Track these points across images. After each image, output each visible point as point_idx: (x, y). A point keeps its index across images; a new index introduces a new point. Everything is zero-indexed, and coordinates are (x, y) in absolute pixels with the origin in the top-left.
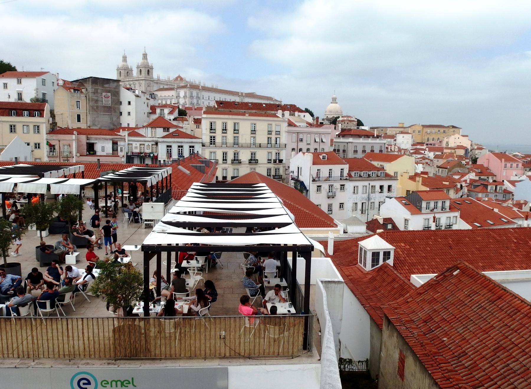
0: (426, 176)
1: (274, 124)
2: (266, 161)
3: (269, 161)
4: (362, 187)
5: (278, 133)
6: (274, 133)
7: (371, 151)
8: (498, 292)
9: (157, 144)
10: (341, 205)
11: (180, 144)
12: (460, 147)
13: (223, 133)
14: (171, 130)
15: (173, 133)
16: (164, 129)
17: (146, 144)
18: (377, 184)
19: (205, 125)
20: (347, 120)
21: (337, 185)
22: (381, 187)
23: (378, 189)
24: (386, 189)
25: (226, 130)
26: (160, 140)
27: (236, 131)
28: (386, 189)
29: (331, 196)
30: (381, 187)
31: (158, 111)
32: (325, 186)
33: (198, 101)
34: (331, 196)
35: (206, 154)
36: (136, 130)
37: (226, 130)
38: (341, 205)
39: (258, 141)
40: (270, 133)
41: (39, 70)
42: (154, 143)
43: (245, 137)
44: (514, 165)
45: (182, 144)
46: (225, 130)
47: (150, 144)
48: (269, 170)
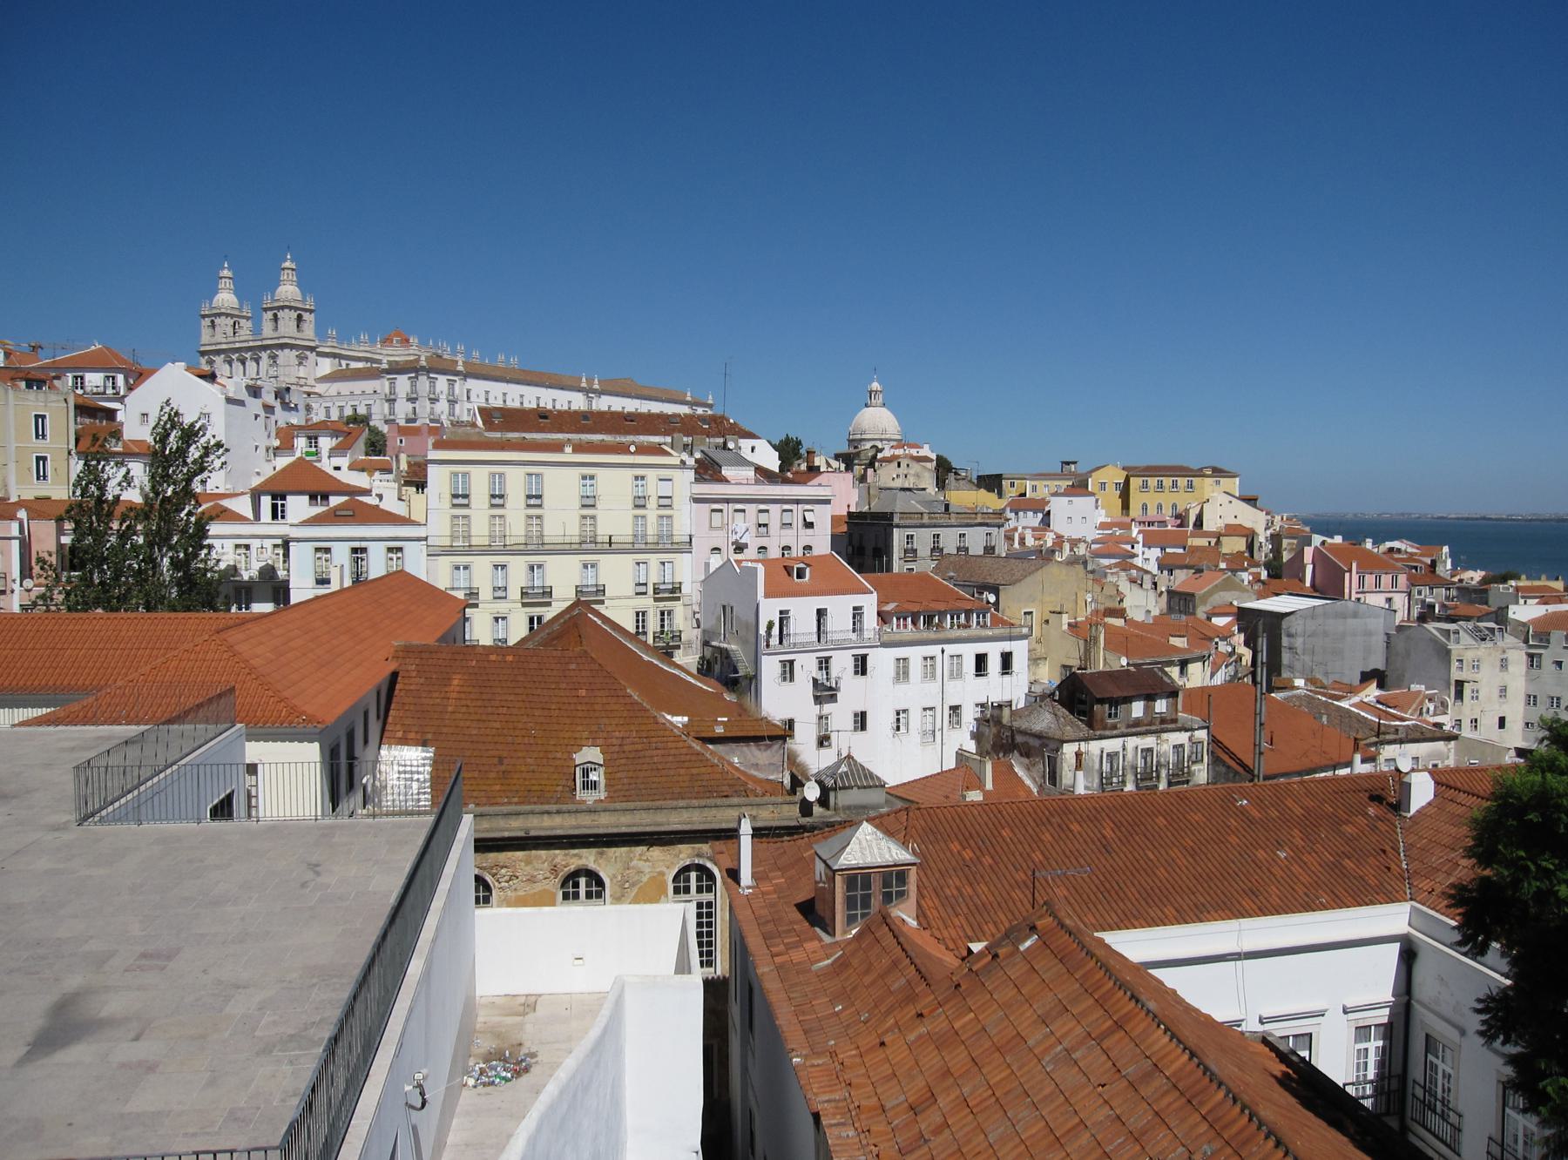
0: (1119, 622)
1: (651, 475)
2: (630, 589)
3: (640, 589)
4: (920, 660)
5: (666, 502)
6: (652, 503)
7: (959, 549)
8: (1134, 989)
9: (286, 545)
10: (861, 721)
11: (357, 544)
12: (1233, 530)
13: (493, 506)
14: (335, 501)
15: (337, 508)
16: (313, 497)
17: (255, 544)
18: (969, 651)
19: (438, 477)
20: (906, 456)
21: (842, 663)
22: (981, 661)
23: (969, 665)
24: (994, 664)
25: (539, 497)
26: (295, 533)
27: (534, 499)
28: (994, 664)
29: (825, 693)
30: (981, 661)
31: (301, 443)
32: (807, 666)
33: (392, 412)
34: (825, 693)
35: (439, 574)
36: (226, 503)
37: (501, 496)
38: (861, 721)
39: (603, 531)
40: (640, 503)
41: (748, 428)
42: (279, 542)
43: (561, 521)
44: (1386, 579)
45: (364, 544)
46: (497, 498)
47: (268, 543)
48: (641, 616)
